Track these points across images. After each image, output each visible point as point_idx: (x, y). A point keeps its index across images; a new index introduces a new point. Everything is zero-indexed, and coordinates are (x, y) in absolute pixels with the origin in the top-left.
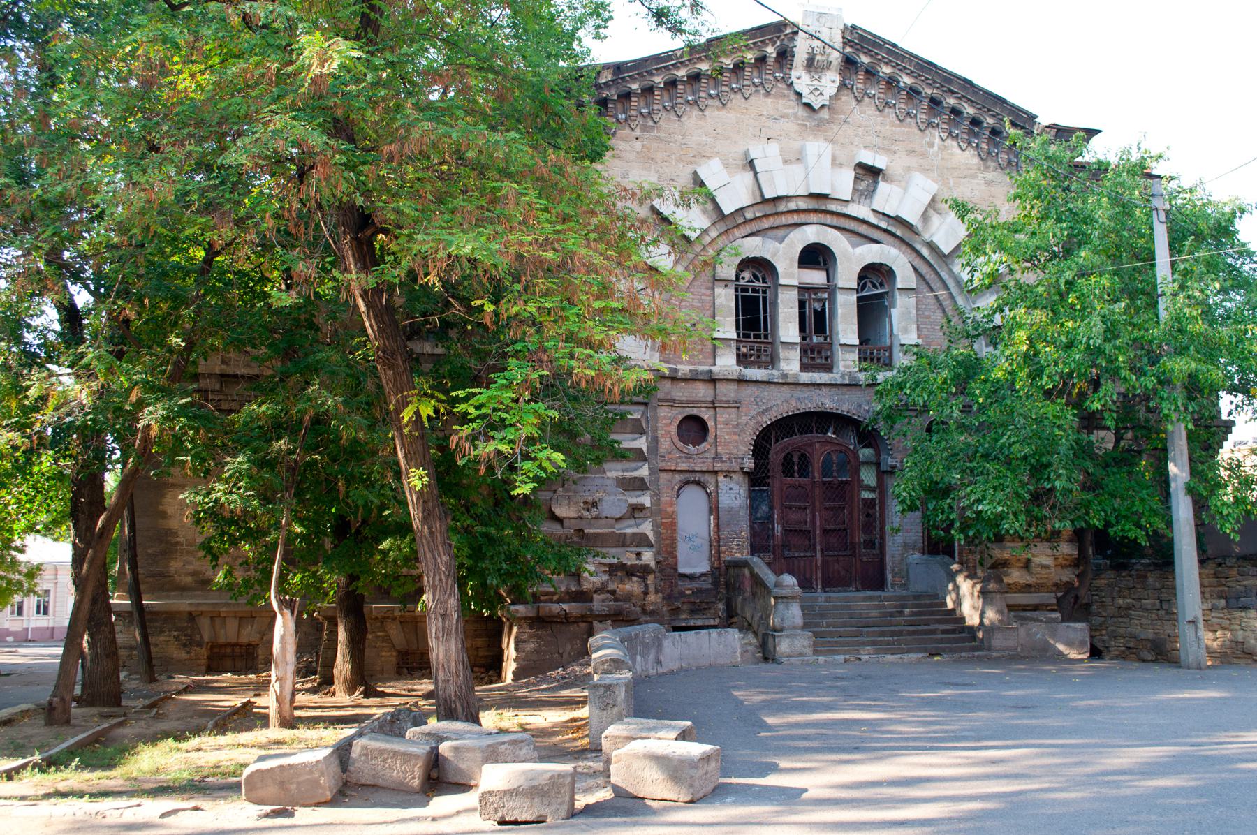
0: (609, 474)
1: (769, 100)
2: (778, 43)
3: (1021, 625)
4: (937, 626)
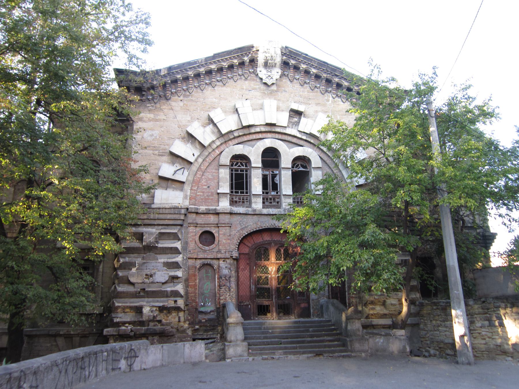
1: (247, 82)
2: (250, 55)
3: (370, 337)
4: (326, 338)
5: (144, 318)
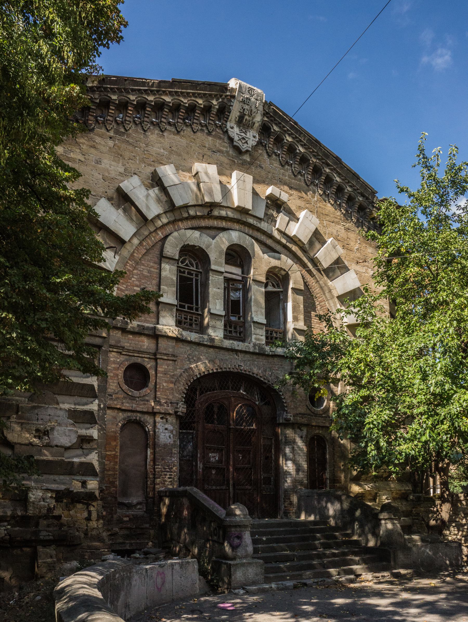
0: (62, 406)
1: (210, 138)
2: (220, 100)
5: (31, 512)
